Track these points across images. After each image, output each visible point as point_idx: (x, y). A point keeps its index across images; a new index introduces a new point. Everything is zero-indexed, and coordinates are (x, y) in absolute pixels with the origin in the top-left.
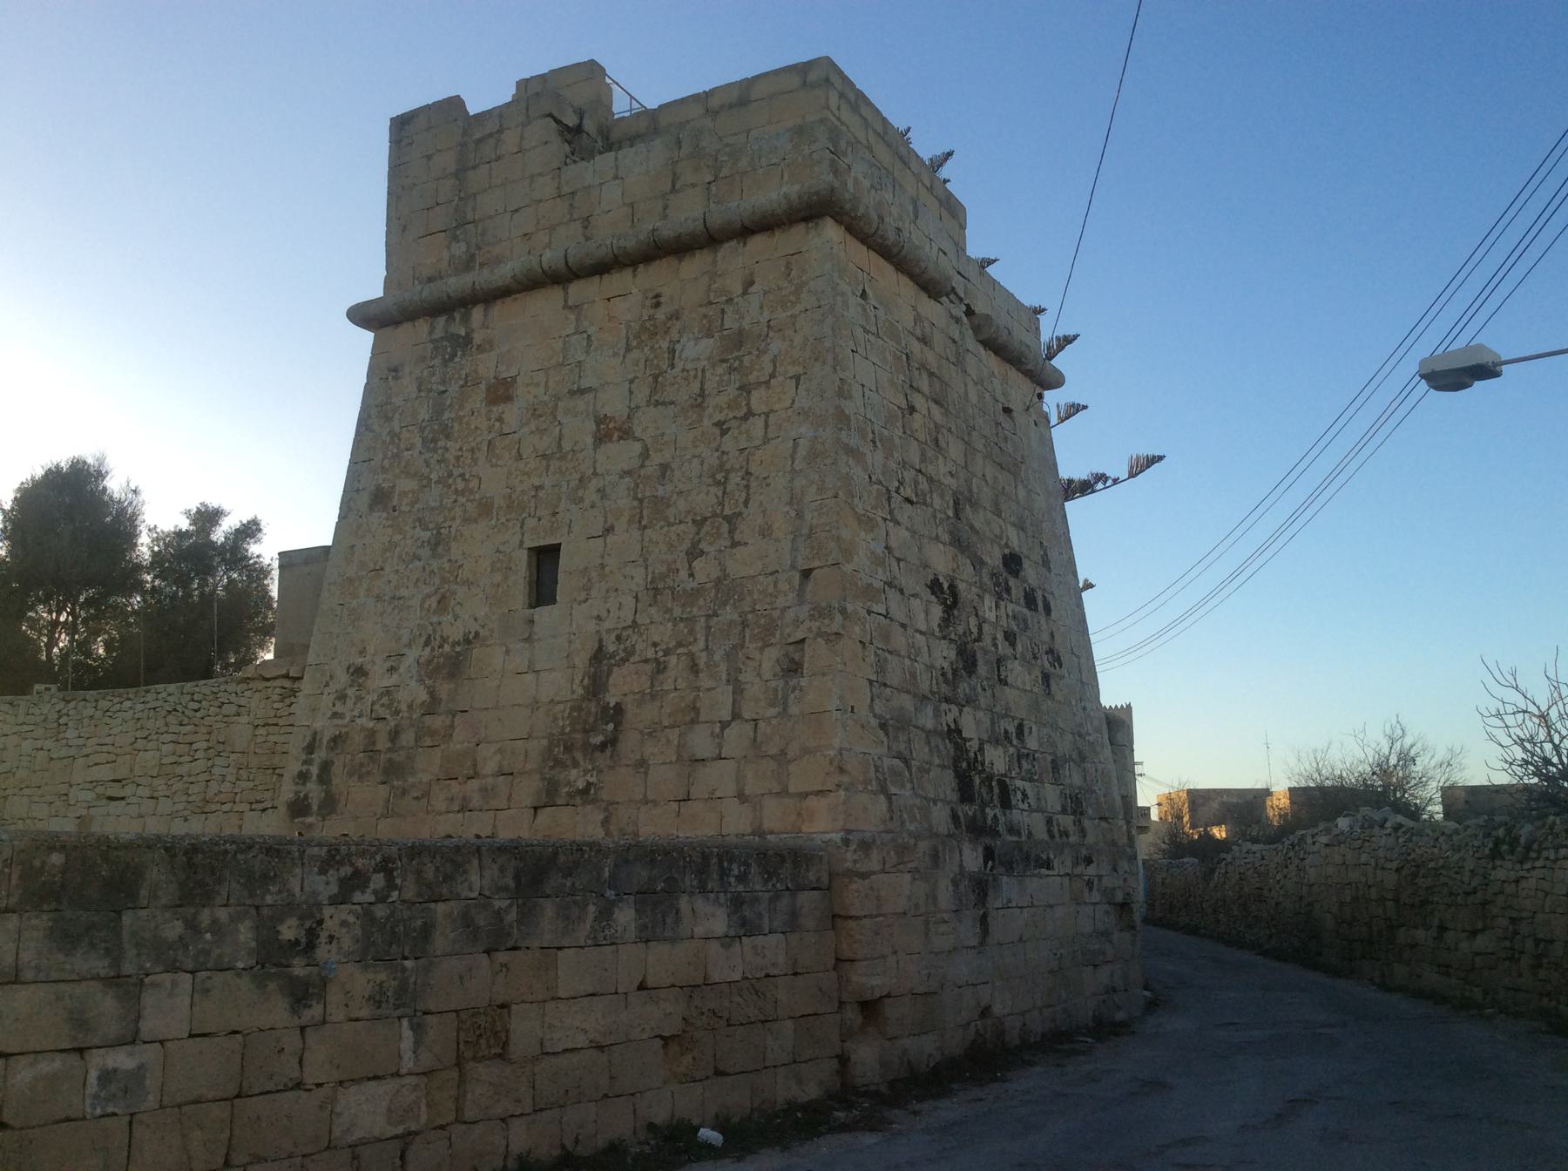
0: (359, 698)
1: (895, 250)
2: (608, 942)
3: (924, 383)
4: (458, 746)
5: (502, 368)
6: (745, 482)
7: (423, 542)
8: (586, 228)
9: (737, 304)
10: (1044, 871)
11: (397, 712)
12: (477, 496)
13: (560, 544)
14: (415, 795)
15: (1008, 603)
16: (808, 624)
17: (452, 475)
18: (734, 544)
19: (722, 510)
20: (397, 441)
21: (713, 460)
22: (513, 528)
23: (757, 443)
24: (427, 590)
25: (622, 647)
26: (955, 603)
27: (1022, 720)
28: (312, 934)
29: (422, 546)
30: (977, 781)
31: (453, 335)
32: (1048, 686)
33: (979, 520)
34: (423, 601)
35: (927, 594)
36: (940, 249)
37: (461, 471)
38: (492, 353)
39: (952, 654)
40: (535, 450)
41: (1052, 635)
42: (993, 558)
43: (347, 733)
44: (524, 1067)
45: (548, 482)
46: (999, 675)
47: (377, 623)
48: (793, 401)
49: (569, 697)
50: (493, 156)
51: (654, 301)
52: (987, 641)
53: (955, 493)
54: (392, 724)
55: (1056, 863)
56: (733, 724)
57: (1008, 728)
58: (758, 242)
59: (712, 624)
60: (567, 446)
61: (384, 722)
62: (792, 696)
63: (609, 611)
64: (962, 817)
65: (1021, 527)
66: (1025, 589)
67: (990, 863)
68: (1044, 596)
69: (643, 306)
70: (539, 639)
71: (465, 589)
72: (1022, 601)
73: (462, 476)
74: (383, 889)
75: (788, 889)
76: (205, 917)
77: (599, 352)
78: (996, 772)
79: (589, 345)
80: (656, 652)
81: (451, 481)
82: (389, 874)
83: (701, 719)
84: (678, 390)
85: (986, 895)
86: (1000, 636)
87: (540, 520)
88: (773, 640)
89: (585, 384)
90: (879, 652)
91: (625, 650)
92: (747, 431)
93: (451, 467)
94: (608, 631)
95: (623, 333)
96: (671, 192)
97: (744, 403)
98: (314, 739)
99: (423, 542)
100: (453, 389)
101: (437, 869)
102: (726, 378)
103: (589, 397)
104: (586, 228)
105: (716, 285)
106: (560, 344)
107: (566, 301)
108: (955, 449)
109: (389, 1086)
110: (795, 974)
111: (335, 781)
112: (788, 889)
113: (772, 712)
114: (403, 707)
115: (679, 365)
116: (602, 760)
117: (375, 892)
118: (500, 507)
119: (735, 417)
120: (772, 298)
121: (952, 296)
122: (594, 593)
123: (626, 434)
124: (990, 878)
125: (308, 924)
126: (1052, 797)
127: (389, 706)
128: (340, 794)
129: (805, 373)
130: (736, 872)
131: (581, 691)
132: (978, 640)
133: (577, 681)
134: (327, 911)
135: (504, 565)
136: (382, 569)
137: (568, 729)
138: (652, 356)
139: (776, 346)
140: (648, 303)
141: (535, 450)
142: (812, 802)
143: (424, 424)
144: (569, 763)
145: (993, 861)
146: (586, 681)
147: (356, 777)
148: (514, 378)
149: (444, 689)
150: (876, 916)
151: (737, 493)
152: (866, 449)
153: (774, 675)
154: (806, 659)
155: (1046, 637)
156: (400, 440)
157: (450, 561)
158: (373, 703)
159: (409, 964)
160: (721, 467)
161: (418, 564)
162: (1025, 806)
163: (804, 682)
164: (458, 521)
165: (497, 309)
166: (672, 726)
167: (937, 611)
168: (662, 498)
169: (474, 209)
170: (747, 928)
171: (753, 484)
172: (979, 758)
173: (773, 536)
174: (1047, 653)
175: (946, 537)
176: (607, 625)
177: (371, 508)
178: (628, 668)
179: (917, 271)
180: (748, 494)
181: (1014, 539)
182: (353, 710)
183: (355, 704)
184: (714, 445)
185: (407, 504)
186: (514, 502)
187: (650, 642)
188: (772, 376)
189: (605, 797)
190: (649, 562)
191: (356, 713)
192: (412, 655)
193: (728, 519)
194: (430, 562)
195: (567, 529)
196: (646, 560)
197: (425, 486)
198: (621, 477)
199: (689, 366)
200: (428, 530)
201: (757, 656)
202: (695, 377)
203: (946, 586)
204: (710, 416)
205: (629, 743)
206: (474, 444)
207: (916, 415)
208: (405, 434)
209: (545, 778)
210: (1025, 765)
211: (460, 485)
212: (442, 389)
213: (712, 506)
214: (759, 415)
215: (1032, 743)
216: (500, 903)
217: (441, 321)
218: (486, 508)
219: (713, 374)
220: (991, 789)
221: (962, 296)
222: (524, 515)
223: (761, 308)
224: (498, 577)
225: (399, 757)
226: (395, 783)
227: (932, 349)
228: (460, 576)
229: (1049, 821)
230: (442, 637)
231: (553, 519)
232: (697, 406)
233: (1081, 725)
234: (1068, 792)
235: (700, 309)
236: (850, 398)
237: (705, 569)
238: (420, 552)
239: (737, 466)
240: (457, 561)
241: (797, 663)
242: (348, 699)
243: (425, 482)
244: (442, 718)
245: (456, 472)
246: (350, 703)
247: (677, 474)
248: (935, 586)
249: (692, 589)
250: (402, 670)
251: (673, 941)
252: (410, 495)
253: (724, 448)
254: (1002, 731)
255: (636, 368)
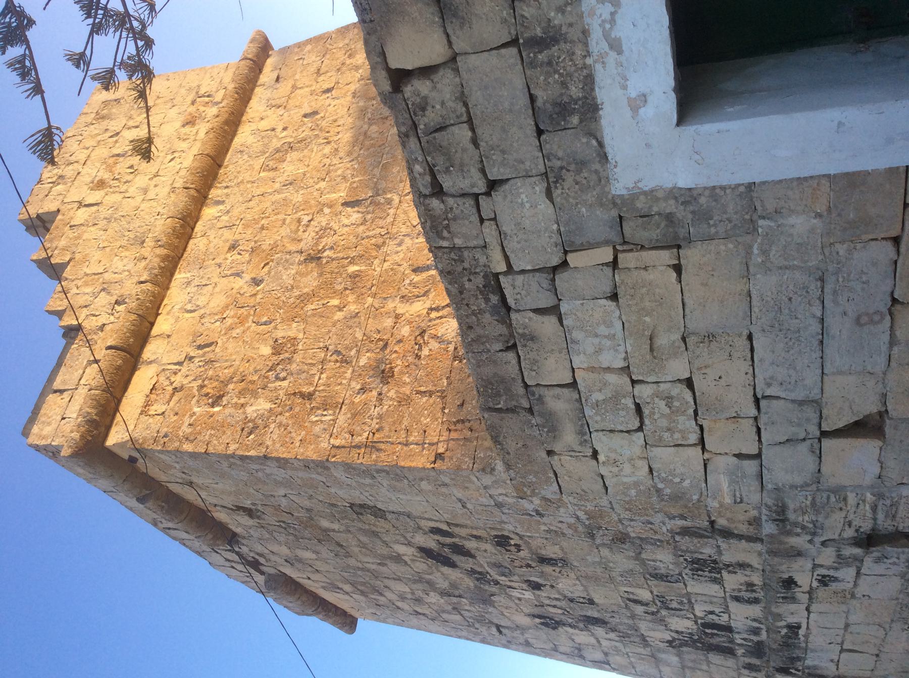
10: (802, 632)
44: (189, 370)
55: (792, 620)
124: (807, 671)
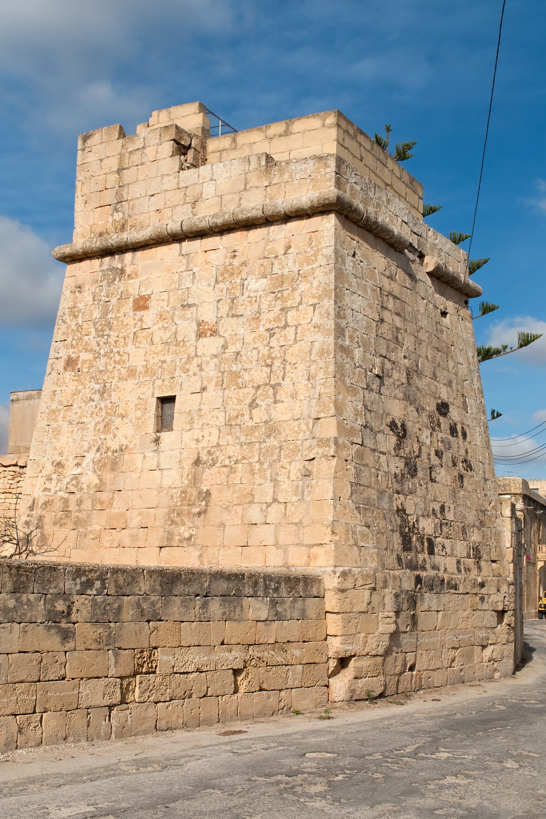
0: (59, 480)
1: (374, 227)
2: (207, 620)
3: (391, 304)
4: (116, 511)
5: (142, 289)
6: (283, 366)
7: (96, 391)
8: (193, 208)
9: (281, 259)
10: (452, 591)
11: (81, 489)
12: (127, 365)
13: (175, 396)
14: (92, 537)
15: (439, 433)
16: (316, 449)
17: (113, 352)
18: (275, 402)
19: (270, 381)
20: (80, 330)
21: (265, 351)
22: (148, 385)
23: (291, 342)
24: (98, 419)
25: (211, 458)
26: (404, 436)
27: (445, 503)
28: (69, 608)
29: (95, 393)
30: (414, 539)
31: (114, 268)
32: (462, 482)
33: (421, 383)
34: (96, 425)
35: (387, 430)
36: (403, 221)
37: (117, 349)
38: (137, 280)
39: (401, 465)
40: (161, 339)
41: (467, 452)
42: (431, 406)
43: (52, 501)
45: (168, 359)
46: (431, 476)
47: (69, 437)
48: (312, 320)
49: (180, 486)
50: (140, 162)
51: (233, 254)
52: (424, 456)
53: (407, 368)
54: (78, 496)
56: (273, 505)
57: (436, 508)
58: (292, 225)
59: (262, 447)
60: (180, 339)
61: (74, 495)
62: (306, 490)
63: (203, 436)
64: (403, 560)
65: (449, 384)
66: (450, 423)
67: (419, 586)
68: (463, 428)
69: (226, 257)
70: (163, 451)
71: (120, 419)
72: (449, 431)
73: (118, 352)
74: (100, 588)
75: (301, 597)
76: (24, 598)
77: (200, 282)
78: (426, 534)
79: (194, 279)
80: (230, 462)
81: (112, 355)
82: (103, 581)
83: (256, 501)
84: (246, 309)
85: (415, 603)
86: (433, 453)
87: (164, 381)
88: (297, 458)
89: (191, 301)
90: (357, 466)
91: (212, 460)
92: (285, 336)
93: (112, 347)
94: (203, 448)
95: (214, 273)
96: (244, 190)
97: (284, 318)
98: (34, 502)
99: (96, 391)
100: (114, 300)
101: (125, 580)
102: (273, 303)
103: (193, 309)
104: (193, 208)
105: (269, 247)
106: (177, 277)
107: (181, 251)
108: (408, 342)
109: (103, 682)
110: (304, 642)
111: (46, 527)
112: (301, 597)
113: (295, 499)
114: (85, 486)
115: (246, 294)
116: (198, 522)
117: (97, 590)
118: (140, 372)
119: (278, 327)
120: (301, 257)
121: (410, 249)
122: (195, 426)
123: (214, 333)
125: (67, 604)
126: (461, 548)
127: (76, 486)
128: (49, 535)
129: (319, 303)
130: (273, 587)
131: (186, 482)
132: (418, 456)
133: (185, 477)
134: (76, 597)
135: (143, 407)
136: (72, 406)
137: (179, 504)
138: (230, 287)
139: (303, 286)
140: (229, 255)
141: (161, 339)
142: (315, 549)
143: (96, 321)
144: (179, 523)
145: (421, 584)
146: (190, 476)
147: (58, 525)
148: (149, 296)
149: (108, 476)
150: (349, 613)
151: (278, 372)
152: (248, 680)
153: (297, 478)
154: (315, 469)
155: (462, 452)
156: (82, 329)
157: (111, 402)
158: (68, 483)
159: (112, 625)
160: (269, 357)
161: (92, 403)
162: (444, 554)
163: (313, 483)
164: (116, 379)
165: (139, 254)
166: (238, 505)
167: (393, 440)
168: (235, 372)
169: (128, 193)
170: (279, 617)
171: (288, 367)
172: (416, 525)
173: (298, 398)
174: (463, 462)
175: (401, 395)
176: (201, 445)
177: (65, 369)
178: (214, 470)
179: (387, 237)
180: (284, 373)
181: (444, 394)
182: (56, 487)
183: (57, 483)
184: (265, 342)
185: (86, 368)
186: (148, 370)
187: (227, 456)
188: (300, 303)
189: (200, 543)
190: (227, 409)
191: (58, 489)
192: (90, 456)
193: (274, 387)
194: (99, 403)
195: (179, 387)
196: (225, 408)
197: (96, 358)
198: (212, 359)
199: (252, 294)
200: (99, 384)
201: (288, 466)
202: (256, 301)
203: (399, 425)
204: (264, 325)
205: (214, 511)
206: (125, 334)
207: (385, 324)
208: (85, 326)
209: (166, 531)
210: (445, 529)
211: (117, 358)
212: (108, 300)
213: (264, 378)
214: (292, 327)
215: (450, 516)
216: (153, 598)
217: (107, 260)
218: (132, 372)
219: (265, 300)
220: (423, 543)
221: (416, 247)
222: (154, 378)
223: (295, 262)
224: (139, 414)
225: (82, 515)
226: (80, 530)
227: (396, 281)
228: (117, 412)
229: (458, 562)
230: (106, 447)
231: (172, 381)
232: (256, 319)
233: (482, 505)
234: (471, 545)
235: (259, 261)
236: (344, 318)
237: (259, 415)
238: (94, 396)
239: (279, 355)
240: (115, 403)
241: (310, 472)
242: (53, 481)
243: (96, 355)
244: (107, 494)
245: (115, 350)
246: (54, 482)
247: (244, 358)
248: (393, 425)
249: (252, 426)
250: (84, 464)
251: (239, 621)
252: (88, 362)
253: (272, 344)
254: (431, 510)
255: (221, 294)
